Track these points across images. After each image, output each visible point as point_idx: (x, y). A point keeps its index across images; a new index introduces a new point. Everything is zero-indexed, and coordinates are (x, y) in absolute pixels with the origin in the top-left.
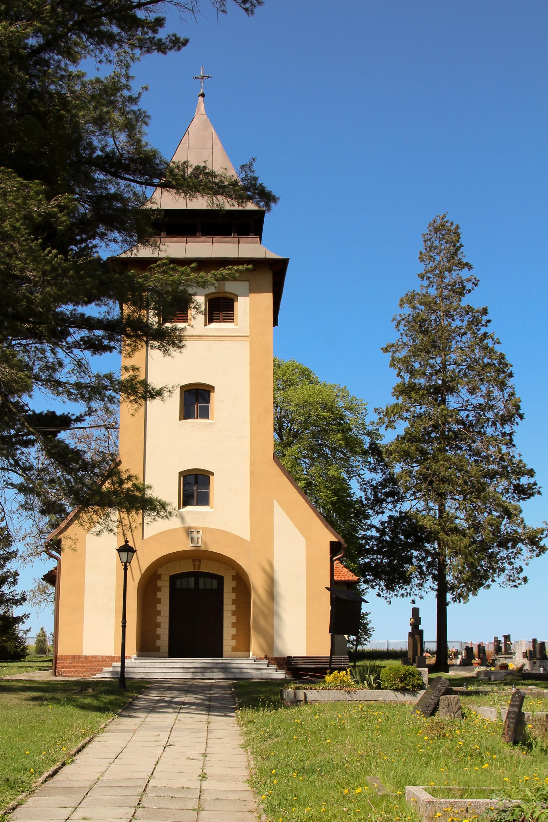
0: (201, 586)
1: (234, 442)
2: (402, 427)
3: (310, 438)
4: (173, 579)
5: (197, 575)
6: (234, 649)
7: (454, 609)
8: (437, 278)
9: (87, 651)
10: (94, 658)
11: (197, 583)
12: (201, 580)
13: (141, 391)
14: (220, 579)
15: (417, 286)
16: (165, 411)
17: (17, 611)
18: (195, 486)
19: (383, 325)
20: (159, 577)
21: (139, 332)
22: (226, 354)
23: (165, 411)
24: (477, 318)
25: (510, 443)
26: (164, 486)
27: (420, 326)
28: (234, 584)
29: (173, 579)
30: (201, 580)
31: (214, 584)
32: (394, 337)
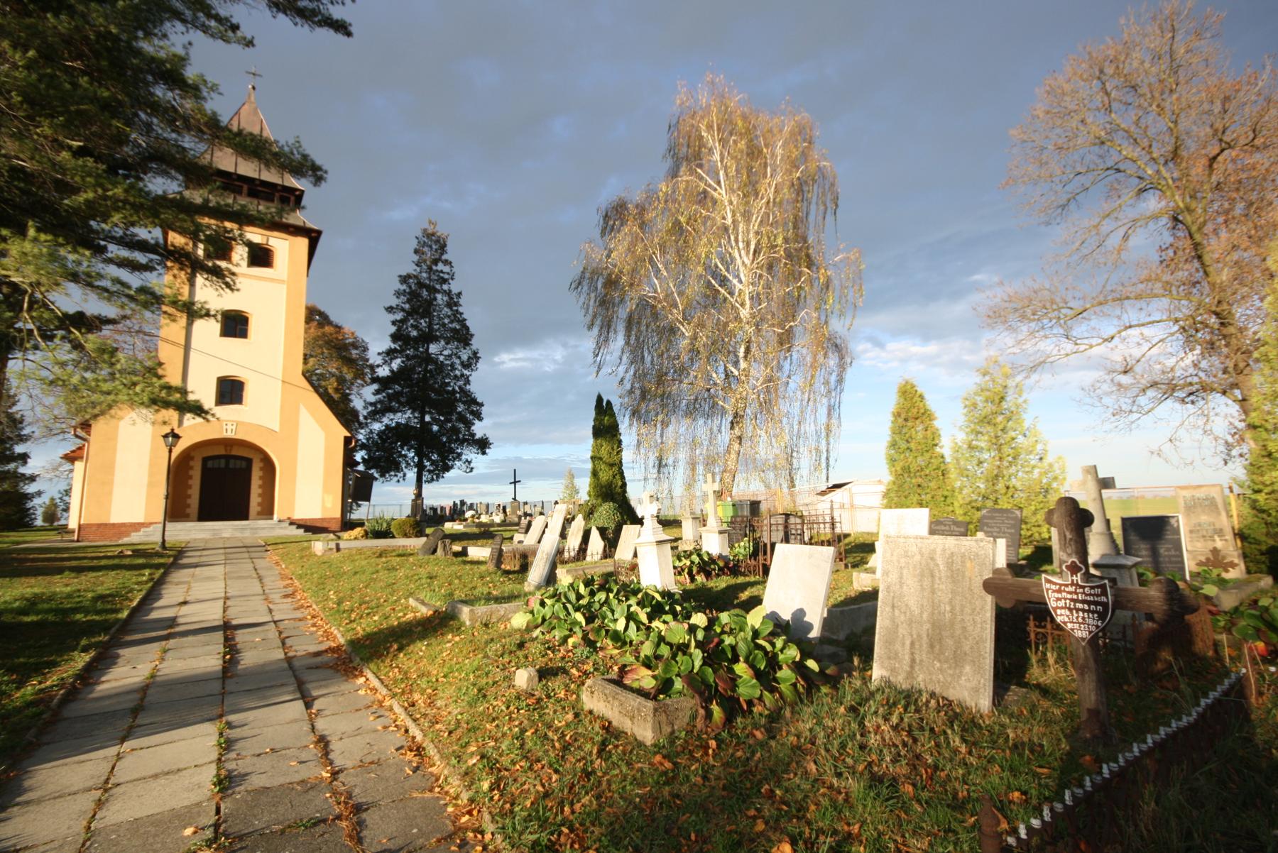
0: (231, 466)
1: (270, 360)
2: (396, 364)
3: (330, 358)
4: (205, 460)
5: (228, 458)
6: (259, 514)
7: (427, 488)
8: (1033, 520)
9: (115, 519)
10: (123, 525)
11: (227, 464)
12: (232, 461)
13: (192, 312)
14: (249, 462)
15: (411, 269)
16: (206, 330)
17: (31, 488)
18: (230, 391)
19: (388, 290)
20: (192, 458)
21: (194, 266)
22: (273, 292)
23: (206, 330)
24: (453, 302)
25: (468, 382)
26: (203, 390)
27: (413, 296)
28: (261, 465)
29: (205, 460)
30: (232, 461)
31: (244, 464)
32: (394, 302)
